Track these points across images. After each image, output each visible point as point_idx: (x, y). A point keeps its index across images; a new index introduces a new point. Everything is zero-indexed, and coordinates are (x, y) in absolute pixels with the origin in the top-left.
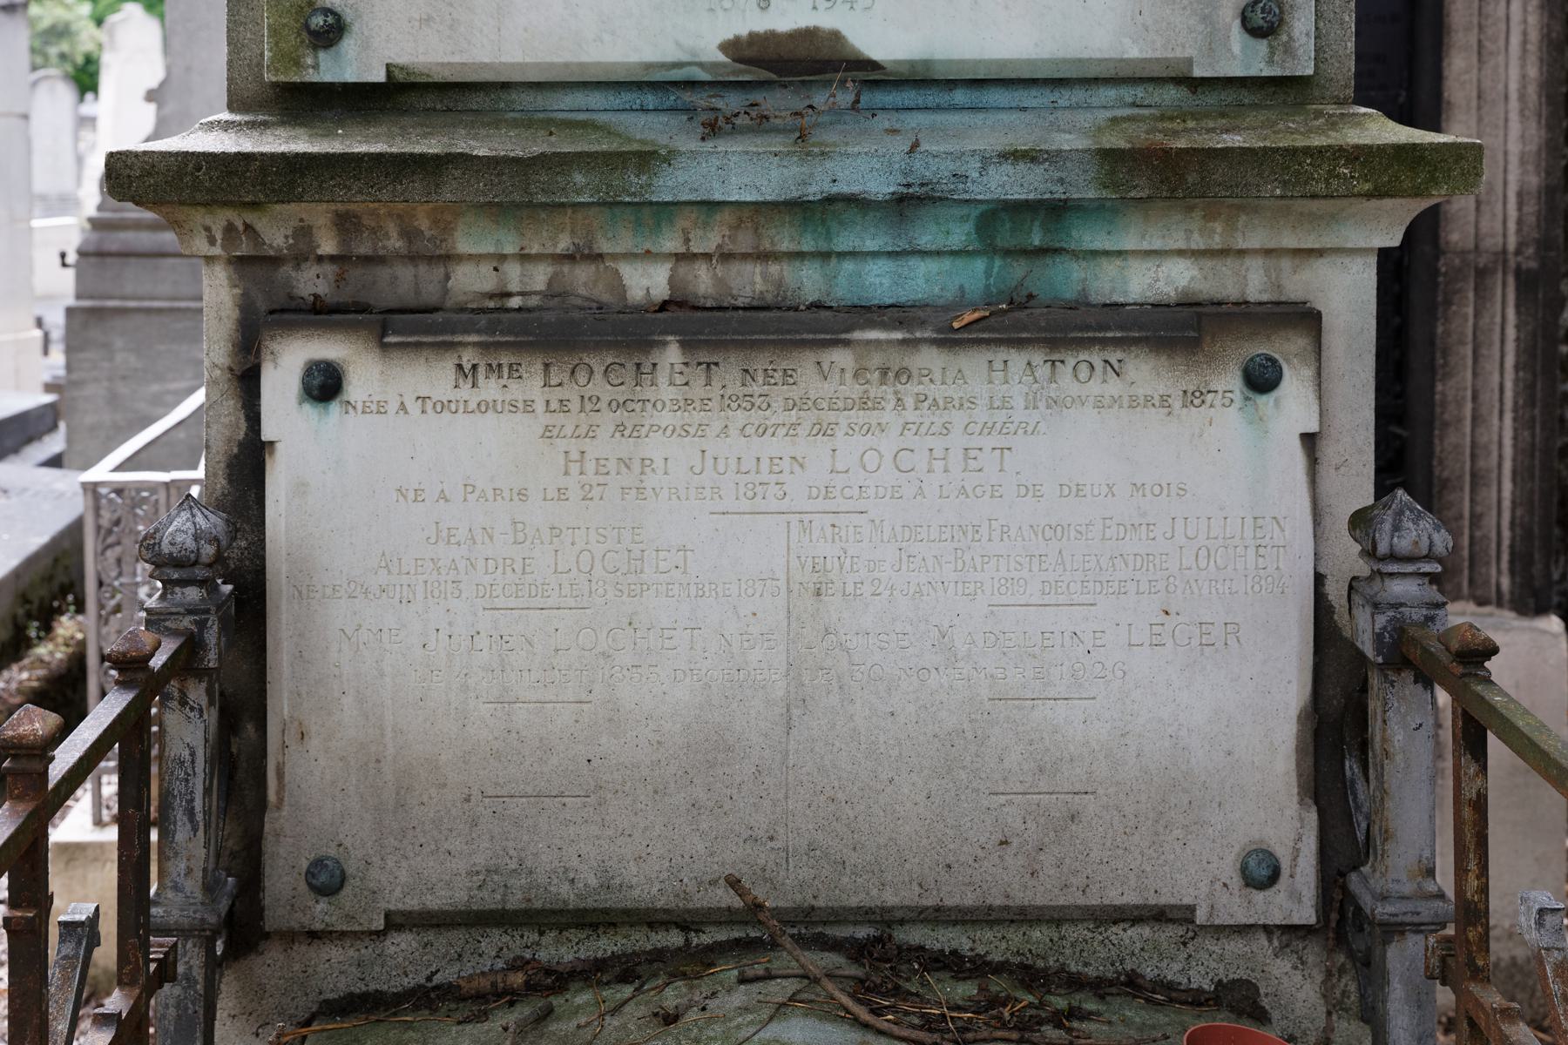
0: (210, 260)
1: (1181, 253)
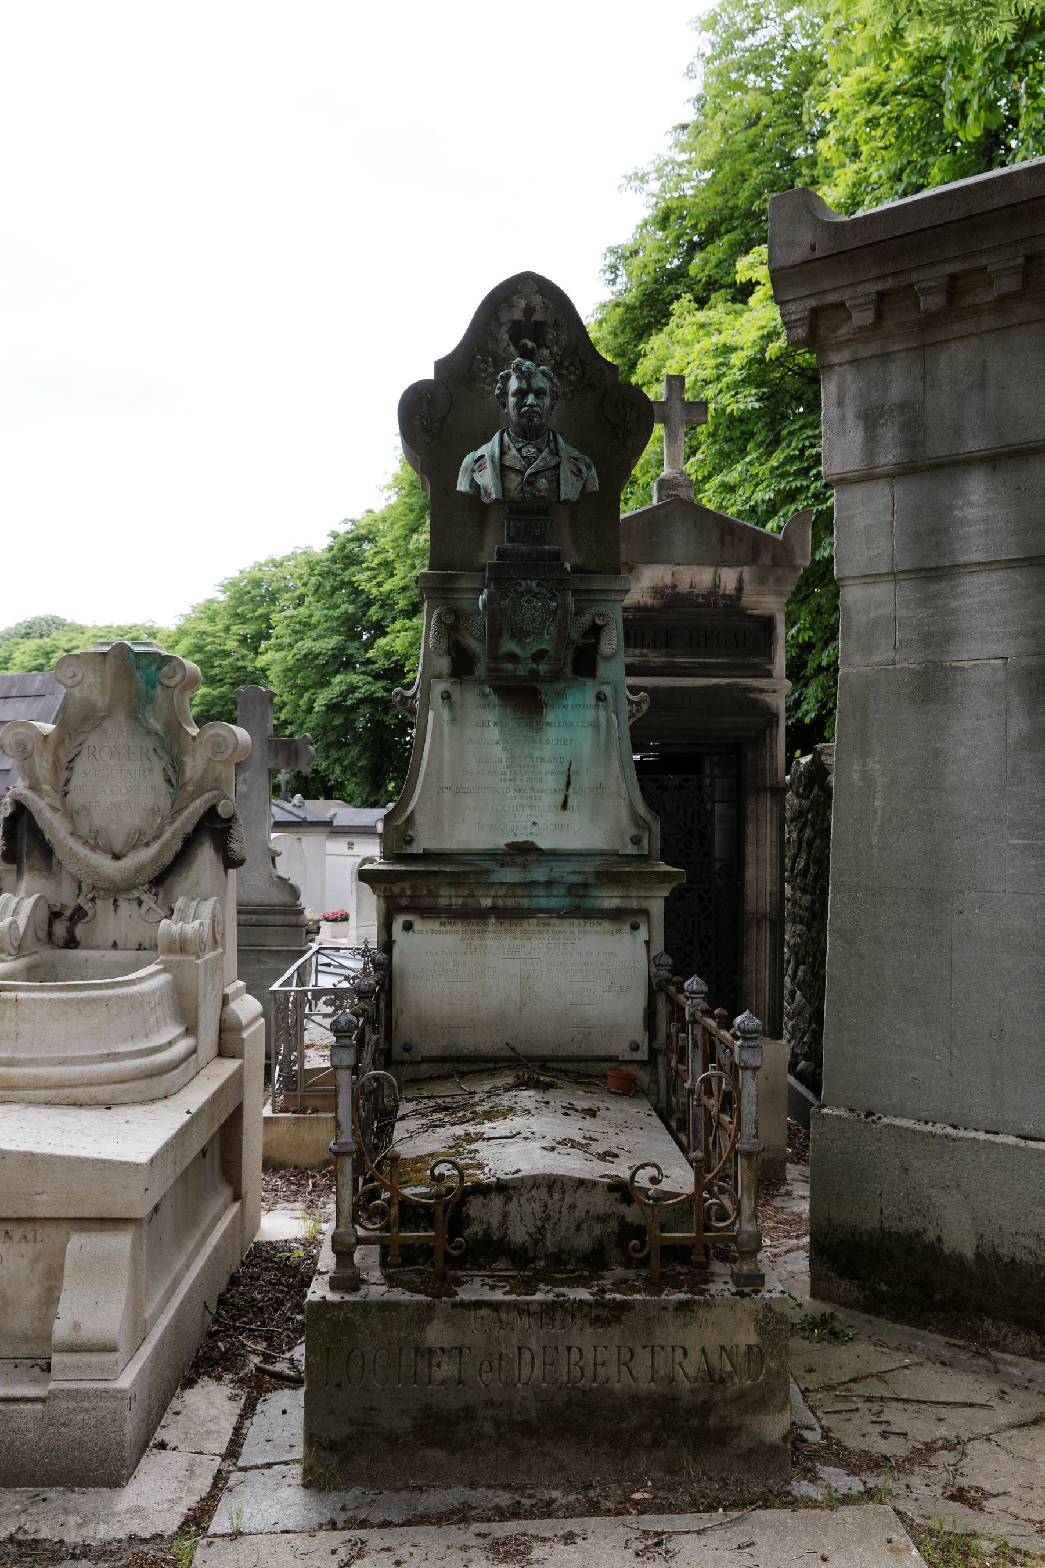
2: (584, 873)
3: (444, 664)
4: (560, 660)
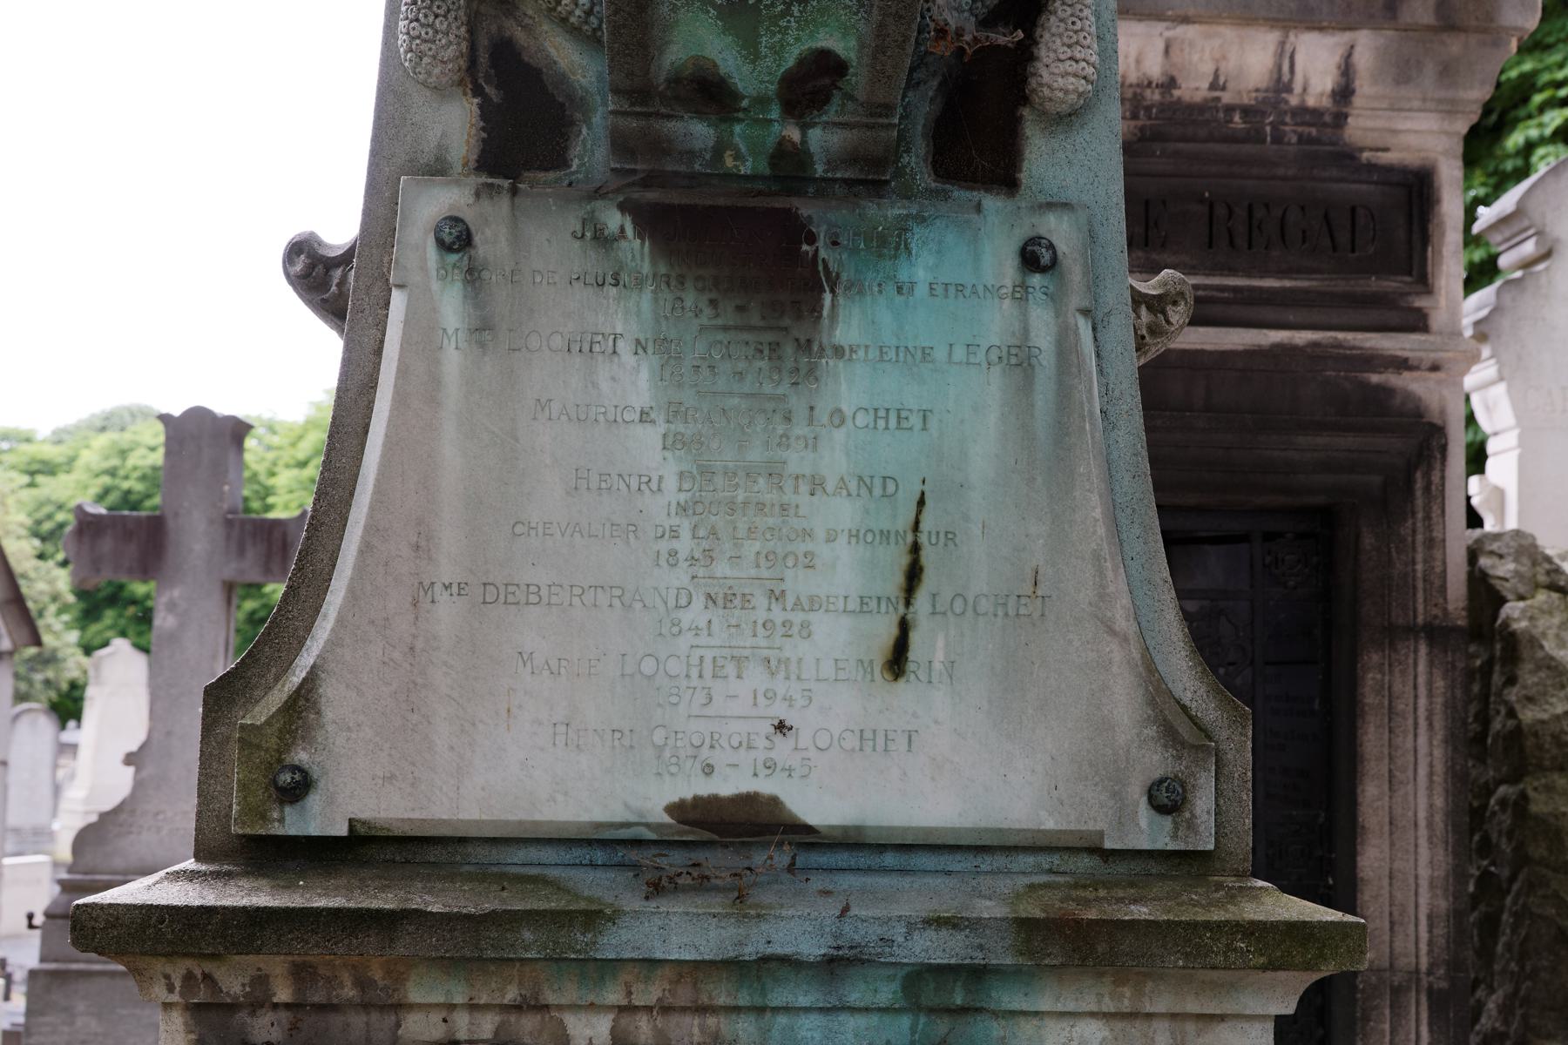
0: (167, 1006)
1: (1092, 1015)
2: (975, 925)
3: (455, 124)
4: (887, 109)
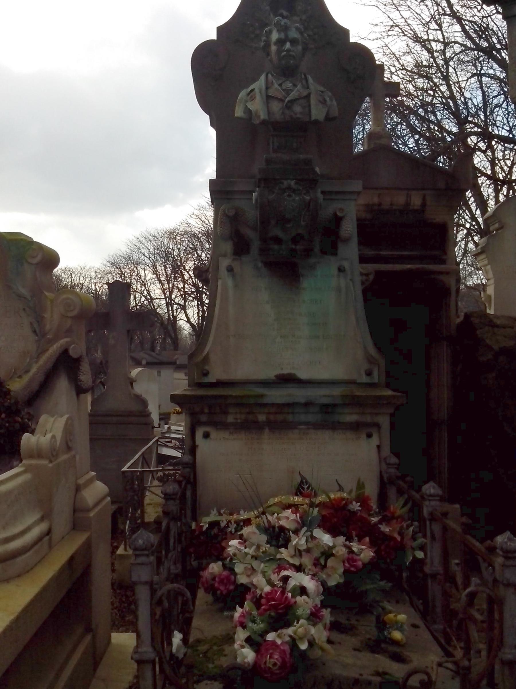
3: (228, 247)
